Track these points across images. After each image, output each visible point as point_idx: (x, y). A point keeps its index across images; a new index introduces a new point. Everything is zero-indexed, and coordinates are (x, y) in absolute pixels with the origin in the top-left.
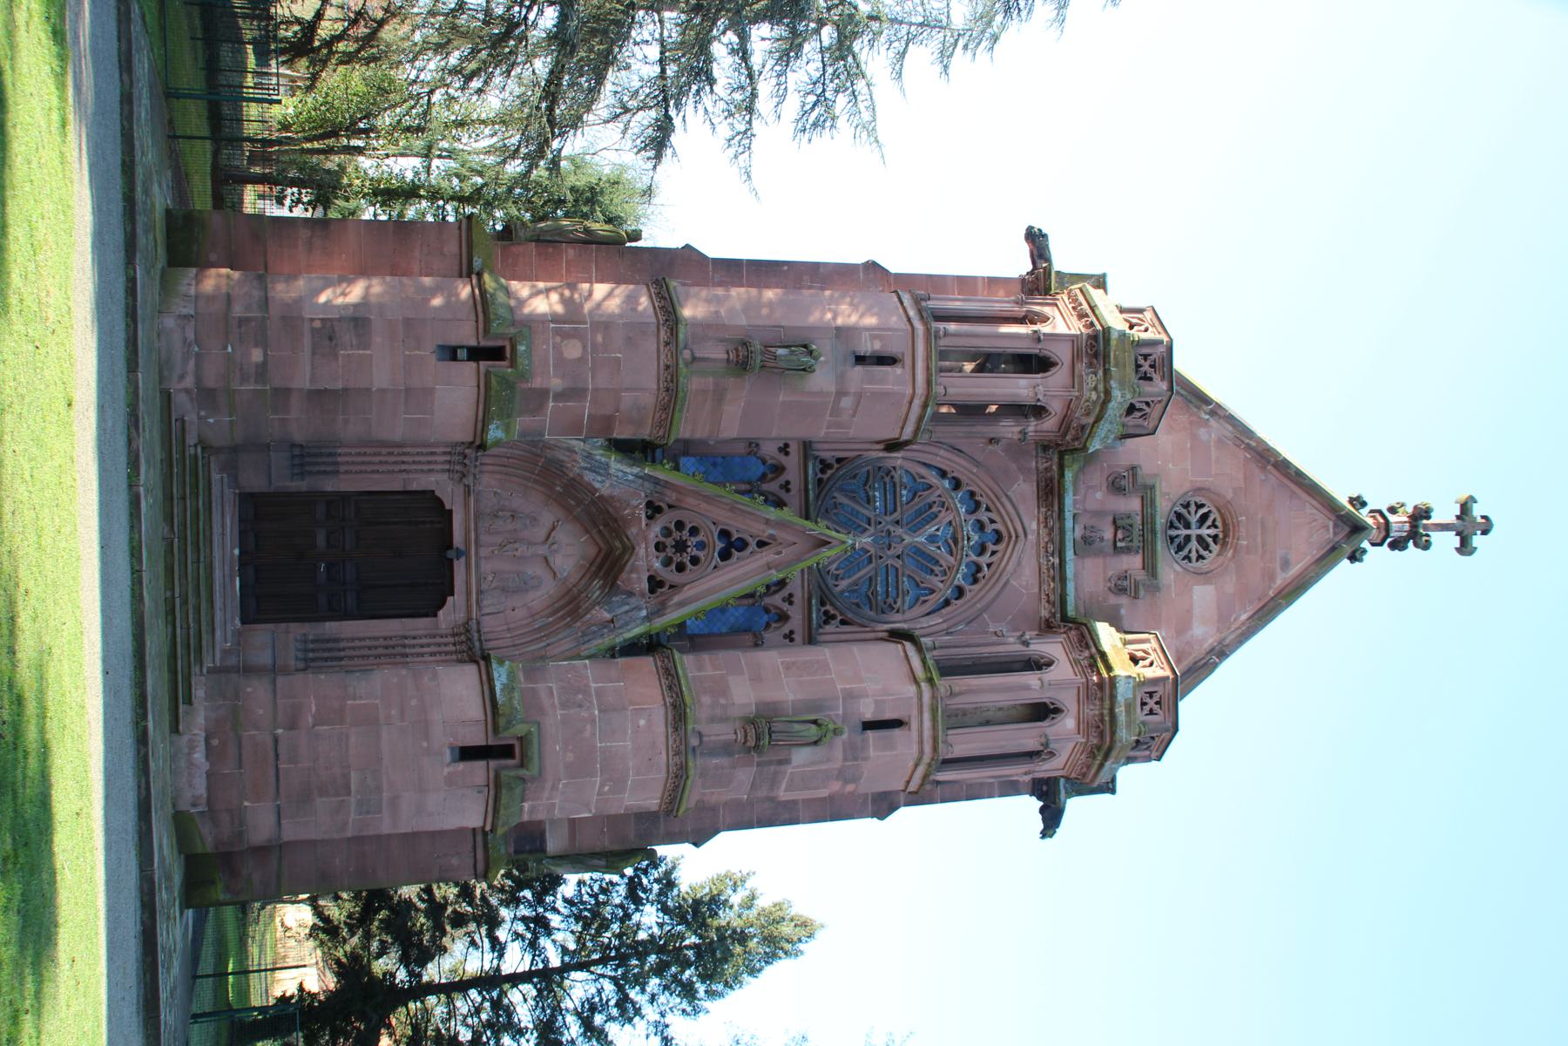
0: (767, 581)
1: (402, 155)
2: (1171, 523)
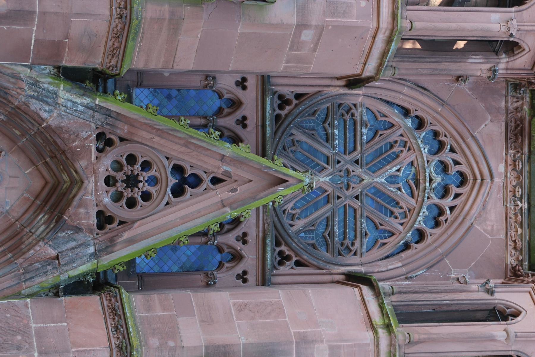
0: (220, 219)
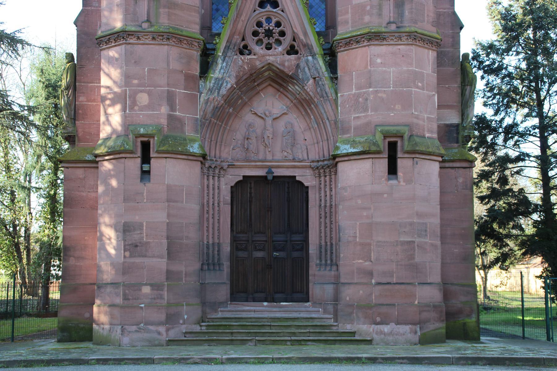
1: (29, 205)
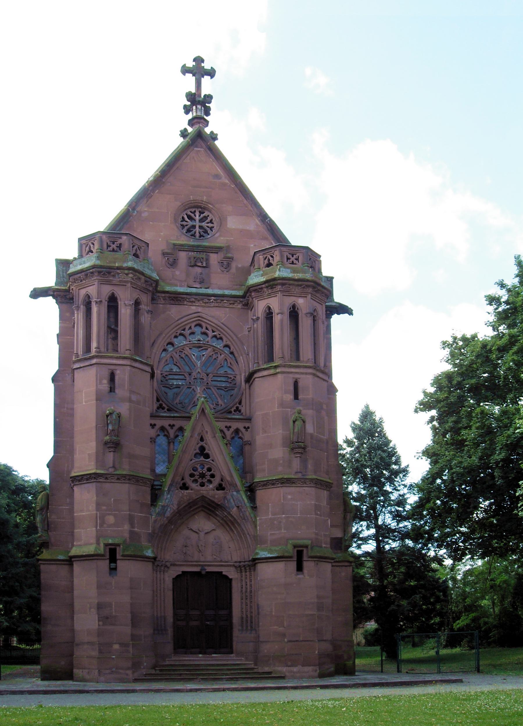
2: (192, 235)
